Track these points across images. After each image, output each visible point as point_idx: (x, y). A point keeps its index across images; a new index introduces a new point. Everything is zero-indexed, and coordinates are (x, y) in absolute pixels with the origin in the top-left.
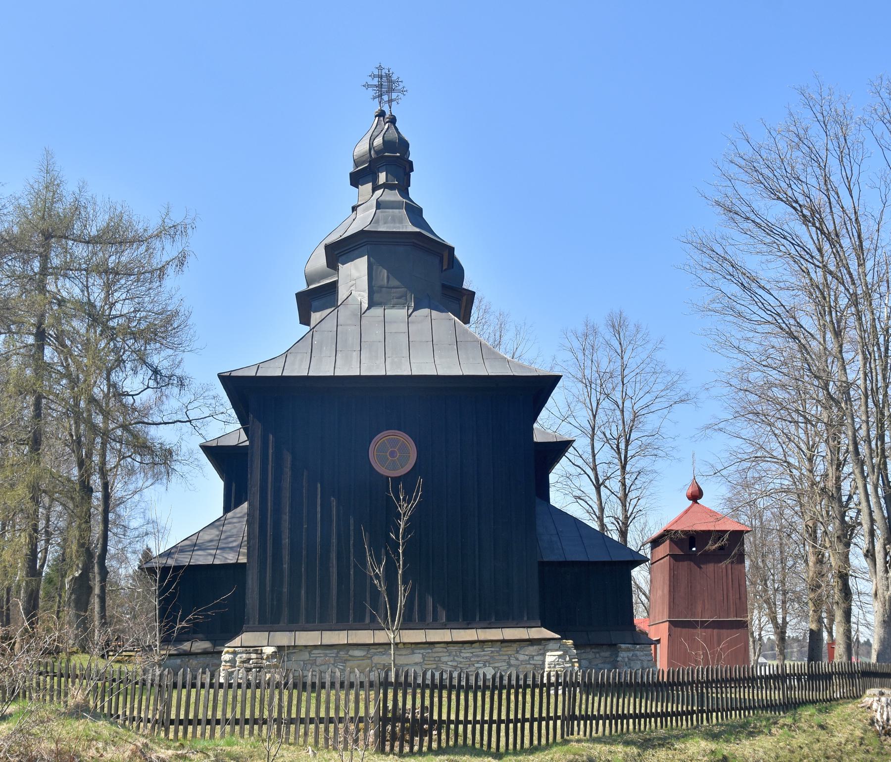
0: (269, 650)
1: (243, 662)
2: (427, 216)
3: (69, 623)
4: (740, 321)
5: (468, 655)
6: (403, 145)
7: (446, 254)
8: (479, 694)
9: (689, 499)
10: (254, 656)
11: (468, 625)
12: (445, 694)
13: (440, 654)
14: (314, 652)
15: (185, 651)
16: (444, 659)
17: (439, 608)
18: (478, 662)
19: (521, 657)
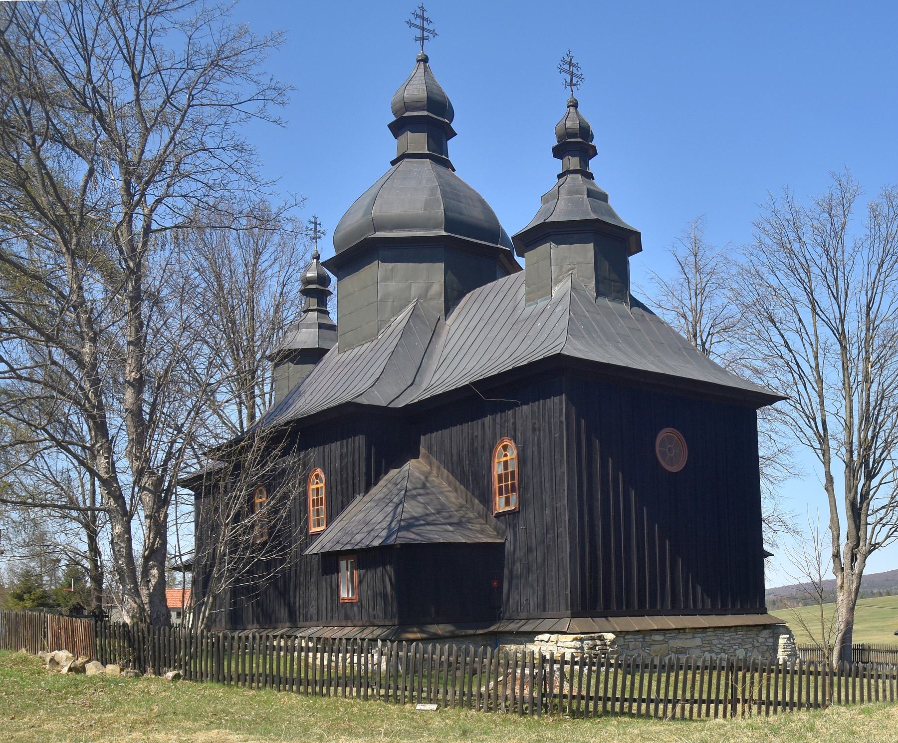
0: (610, 637)
1: (590, 649)
2: (613, 203)
3: (40, 576)
4: (864, 310)
5: (728, 638)
6: (585, 132)
7: (632, 239)
8: (673, 674)
9: (559, 152)
10: (598, 642)
11: (724, 612)
12: (715, 674)
13: (711, 638)
14: (628, 637)
15: (435, 634)
16: (715, 642)
17: (705, 597)
18: (735, 644)
19: (761, 640)
